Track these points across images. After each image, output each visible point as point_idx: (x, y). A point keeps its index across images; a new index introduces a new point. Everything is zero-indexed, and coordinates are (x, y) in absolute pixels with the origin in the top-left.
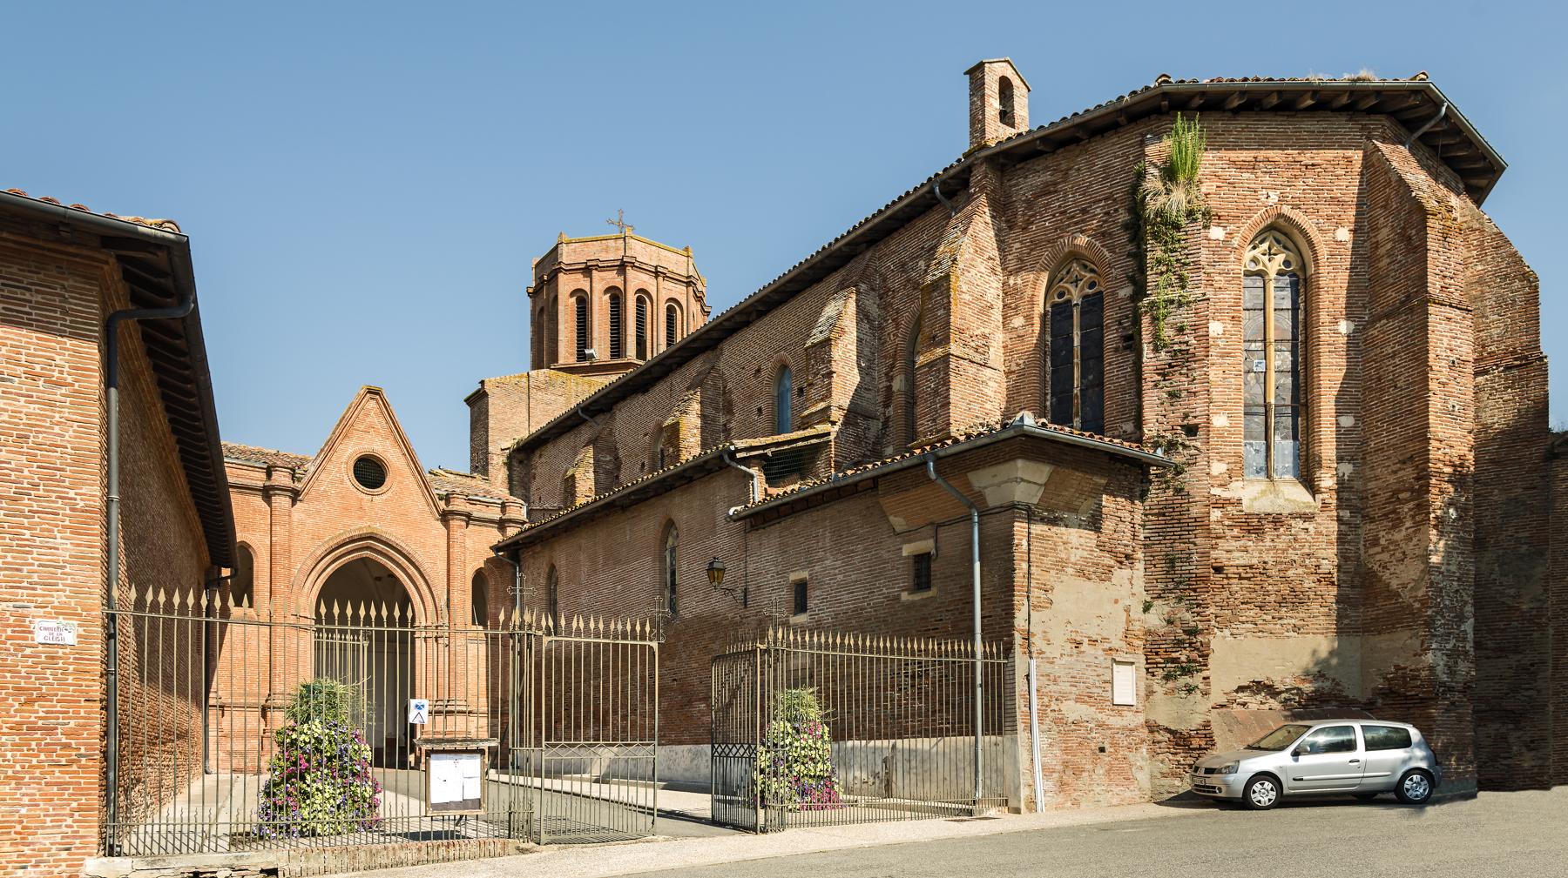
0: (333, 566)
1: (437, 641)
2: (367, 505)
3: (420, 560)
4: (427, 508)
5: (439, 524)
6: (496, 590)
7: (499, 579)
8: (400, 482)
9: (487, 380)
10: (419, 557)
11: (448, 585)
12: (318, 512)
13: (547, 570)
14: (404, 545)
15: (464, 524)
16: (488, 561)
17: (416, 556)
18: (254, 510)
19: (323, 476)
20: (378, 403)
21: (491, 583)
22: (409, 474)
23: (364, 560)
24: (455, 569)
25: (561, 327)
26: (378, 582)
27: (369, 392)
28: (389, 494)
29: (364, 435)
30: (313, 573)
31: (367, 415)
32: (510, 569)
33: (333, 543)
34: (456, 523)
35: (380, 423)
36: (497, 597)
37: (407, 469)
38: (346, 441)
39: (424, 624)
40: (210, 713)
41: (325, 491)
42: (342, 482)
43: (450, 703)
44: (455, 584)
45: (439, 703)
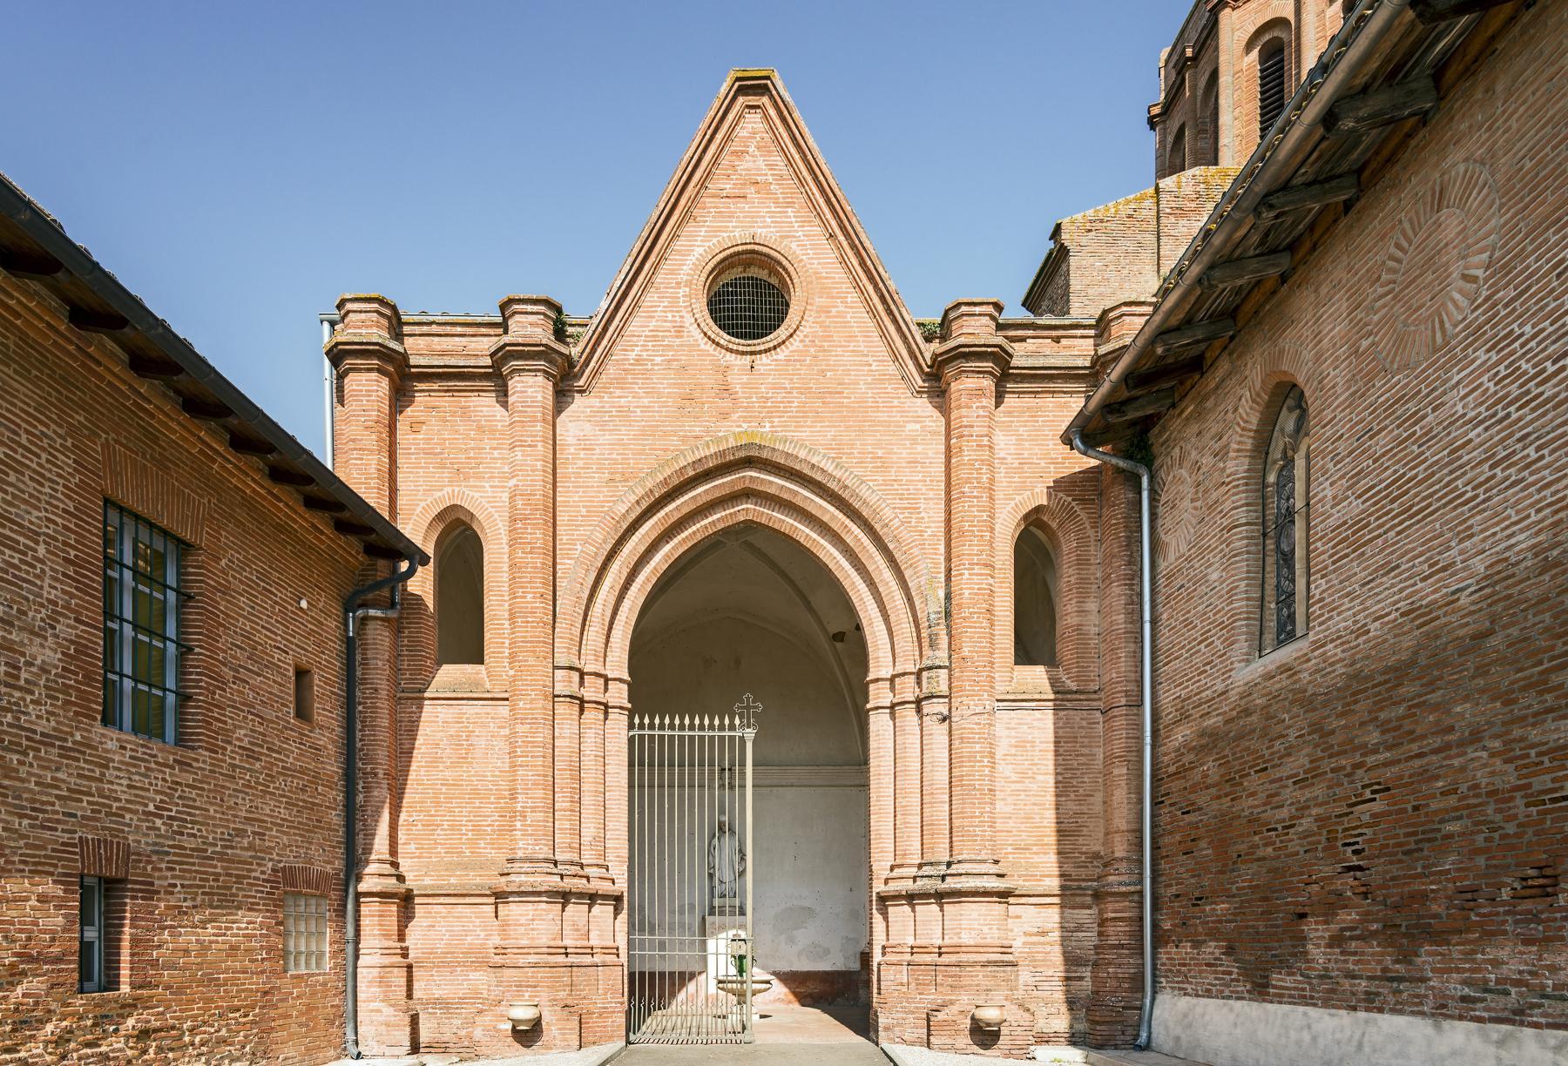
0: (667, 548)
1: (919, 710)
2: (738, 380)
3: (873, 499)
4: (892, 369)
5: (924, 406)
6: (1082, 562)
7: (1091, 533)
8: (825, 310)
9: (1065, 221)
10: (870, 494)
11: (949, 559)
12: (624, 413)
13: (1254, 420)
14: (830, 468)
15: (988, 383)
16: (1063, 486)
17: (863, 492)
18: (480, 429)
19: (635, 325)
20: (766, 117)
21: (1068, 546)
22: (846, 286)
23: (750, 526)
24: (969, 511)
25: (1225, 118)
26: (839, 645)
27: (742, 91)
28: (795, 344)
29: (733, 205)
30: (615, 566)
31: (740, 154)
32: (1121, 494)
33: (653, 481)
34: (971, 386)
35: (771, 167)
36: (1083, 582)
37: (840, 274)
38: (689, 229)
39: (887, 672)
40: (364, 909)
41: (638, 361)
42: (679, 331)
43: (954, 869)
44: (967, 549)
45: (927, 870)
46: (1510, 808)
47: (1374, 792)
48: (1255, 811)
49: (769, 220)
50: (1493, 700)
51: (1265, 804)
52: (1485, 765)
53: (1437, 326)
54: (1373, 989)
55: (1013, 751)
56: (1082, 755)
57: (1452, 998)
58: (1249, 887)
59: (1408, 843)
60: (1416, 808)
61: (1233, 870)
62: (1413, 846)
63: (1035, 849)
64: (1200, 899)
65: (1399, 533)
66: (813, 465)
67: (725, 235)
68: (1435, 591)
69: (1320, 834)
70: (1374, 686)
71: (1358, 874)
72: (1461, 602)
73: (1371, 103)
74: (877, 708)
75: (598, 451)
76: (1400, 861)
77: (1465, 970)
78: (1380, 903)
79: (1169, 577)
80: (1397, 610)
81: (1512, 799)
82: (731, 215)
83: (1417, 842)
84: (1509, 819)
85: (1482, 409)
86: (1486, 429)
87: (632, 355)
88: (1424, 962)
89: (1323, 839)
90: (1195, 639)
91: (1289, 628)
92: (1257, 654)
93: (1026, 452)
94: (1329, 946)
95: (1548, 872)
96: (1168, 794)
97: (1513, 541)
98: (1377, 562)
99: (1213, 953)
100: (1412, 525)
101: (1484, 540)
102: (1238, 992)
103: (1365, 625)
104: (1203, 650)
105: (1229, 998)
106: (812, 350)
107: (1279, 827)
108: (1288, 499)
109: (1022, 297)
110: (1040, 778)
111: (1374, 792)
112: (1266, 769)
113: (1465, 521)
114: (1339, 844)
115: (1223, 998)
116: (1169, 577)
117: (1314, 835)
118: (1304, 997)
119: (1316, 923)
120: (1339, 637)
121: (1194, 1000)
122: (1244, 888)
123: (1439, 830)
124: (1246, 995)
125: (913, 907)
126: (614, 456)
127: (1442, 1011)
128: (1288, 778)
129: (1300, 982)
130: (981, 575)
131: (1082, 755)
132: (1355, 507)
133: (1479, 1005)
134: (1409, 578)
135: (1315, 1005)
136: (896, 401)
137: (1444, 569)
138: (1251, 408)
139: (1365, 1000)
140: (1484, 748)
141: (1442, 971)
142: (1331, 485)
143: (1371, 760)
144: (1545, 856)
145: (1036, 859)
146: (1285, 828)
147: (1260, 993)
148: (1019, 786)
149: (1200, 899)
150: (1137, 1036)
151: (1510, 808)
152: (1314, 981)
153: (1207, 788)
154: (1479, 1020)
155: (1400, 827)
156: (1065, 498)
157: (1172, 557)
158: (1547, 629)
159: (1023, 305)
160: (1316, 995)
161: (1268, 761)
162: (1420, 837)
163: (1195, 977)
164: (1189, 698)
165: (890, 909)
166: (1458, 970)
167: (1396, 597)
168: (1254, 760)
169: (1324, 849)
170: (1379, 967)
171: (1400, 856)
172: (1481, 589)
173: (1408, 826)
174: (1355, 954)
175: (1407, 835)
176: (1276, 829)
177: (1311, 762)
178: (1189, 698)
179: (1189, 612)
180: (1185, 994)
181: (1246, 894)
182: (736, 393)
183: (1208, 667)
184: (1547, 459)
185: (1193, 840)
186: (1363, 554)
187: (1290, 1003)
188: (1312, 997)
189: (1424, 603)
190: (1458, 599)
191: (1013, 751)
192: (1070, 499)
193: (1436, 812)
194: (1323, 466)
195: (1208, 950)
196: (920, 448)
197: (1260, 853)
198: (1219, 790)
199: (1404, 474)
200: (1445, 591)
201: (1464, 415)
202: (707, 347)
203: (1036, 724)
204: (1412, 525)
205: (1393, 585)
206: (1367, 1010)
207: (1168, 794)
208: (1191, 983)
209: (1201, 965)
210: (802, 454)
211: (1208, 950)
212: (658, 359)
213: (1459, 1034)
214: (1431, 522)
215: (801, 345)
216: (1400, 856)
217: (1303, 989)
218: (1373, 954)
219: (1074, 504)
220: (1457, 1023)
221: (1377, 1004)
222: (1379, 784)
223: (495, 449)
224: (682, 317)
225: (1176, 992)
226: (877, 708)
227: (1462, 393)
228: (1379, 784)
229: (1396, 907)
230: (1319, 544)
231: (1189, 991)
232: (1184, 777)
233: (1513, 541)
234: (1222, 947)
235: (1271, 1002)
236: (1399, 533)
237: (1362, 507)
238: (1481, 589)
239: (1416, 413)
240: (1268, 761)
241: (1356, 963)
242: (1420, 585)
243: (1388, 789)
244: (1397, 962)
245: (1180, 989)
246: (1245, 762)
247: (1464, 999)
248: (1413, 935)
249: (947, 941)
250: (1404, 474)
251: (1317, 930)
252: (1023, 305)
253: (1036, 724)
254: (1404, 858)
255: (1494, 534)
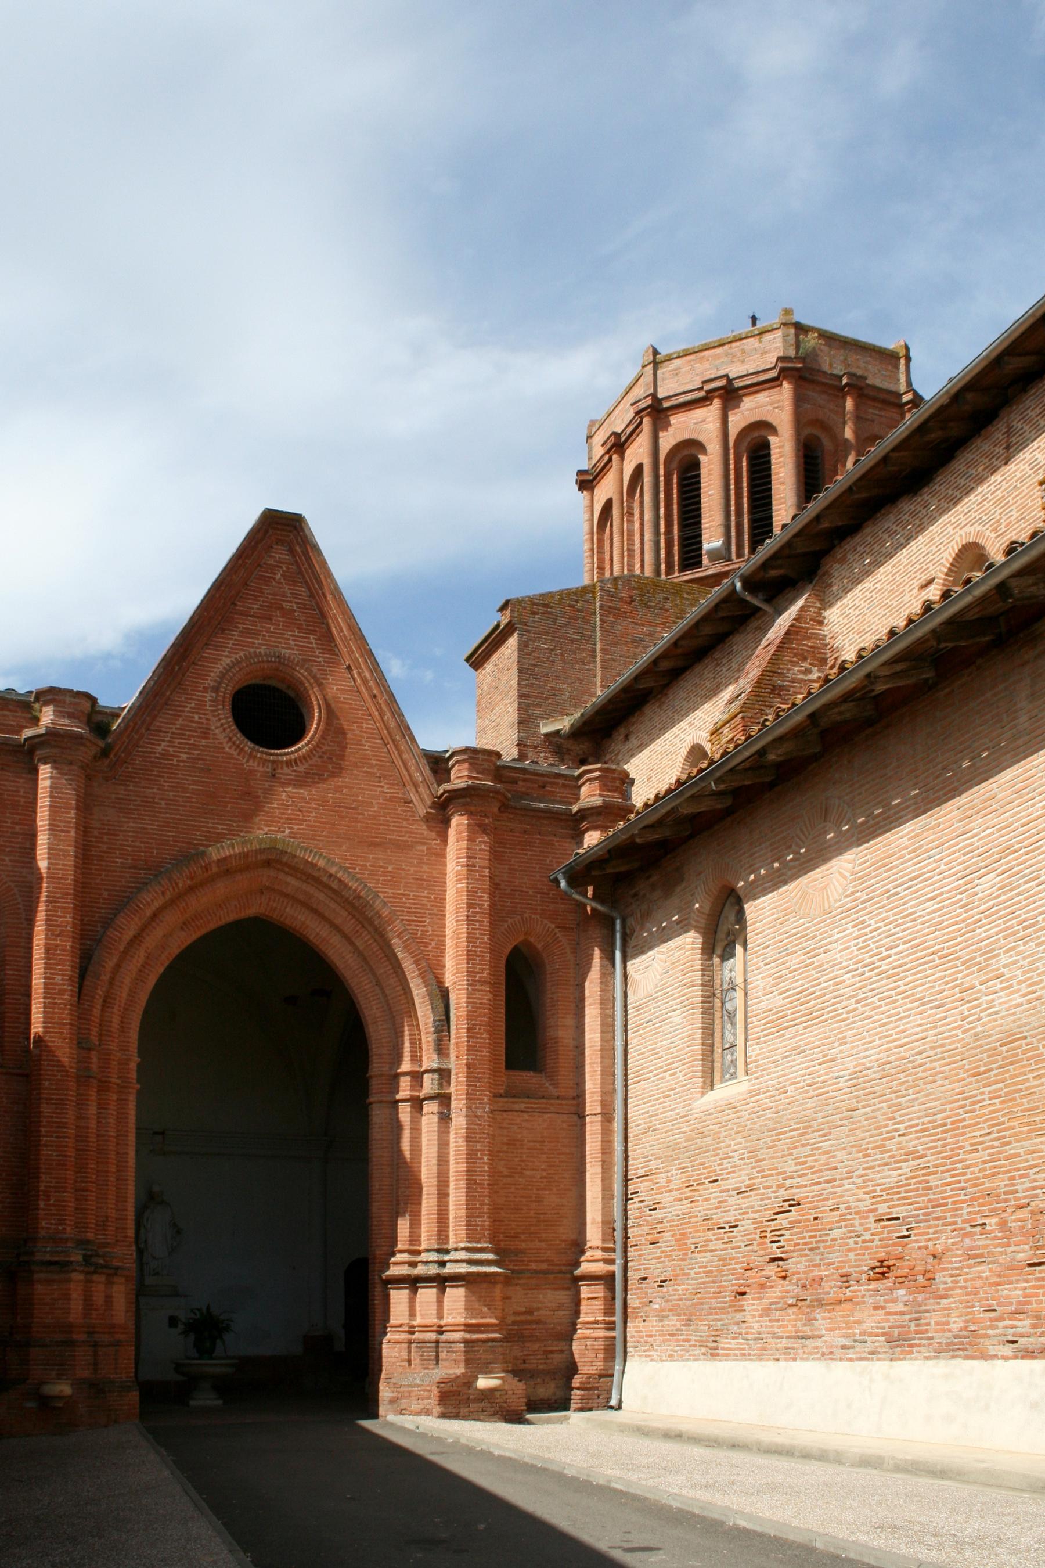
35: (295, 595)
46: (867, 1223)
47: (790, 1205)
48: (709, 1212)
49: (292, 643)
50: (858, 1152)
51: (716, 1208)
52: (854, 1195)
53: (825, 897)
54: (790, 1345)
55: (505, 1148)
56: (563, 1154)
57: (837, 1347)
58: (705, 1272)
59: (811, 1243)
60: (816, 1219)
61: (691, 1259)
62: (814, 1245)
63: (523, 1237)
64: (664, 1281)
65: (805, 1028)
66: (331, 875)
67: (252, 650)
68: (826, 1074)
69: (756, 1234)
70: (791, 1131)
71: (781, 1263)
72: (840, 1084)
73: (785, 746)
74: (381, 1102)
75: (121, 837)
76: (807, 1255)
77: (843, 1328)
78: (794, 1284)
79: (638, 1008)
80: (804, 1080)
81: (867, 1217)
82: (258, 633)
83: (816, 1242)
84: (867, 1230)
85: (851, 962)
86: (853, 977)
87: (159, 749)
88: (820, 1325)
89: (757, 1237)
90: (661, 1067)
91: (732, 1071)
92: (709, 1088)
93: (517, 881)
94: (761, 1316)
95: (885, 1264)
96: (637, 1192)
97: (867, 1053)
98: (792, 1044)
99: (674, 1325)
100: (813, 1025)
101: (853, 1048)
102: (694, 1355)
103: (784, 1086)
104: (669, 1078)
105: (688, 1360)
106: (330, 766)
107: (727, 1226)
108: (731, 971)
109: (468, 652)
110: (528, 1173)
111: (790, 1205)
112: (716, 1181)
113: (842, 1032)
114: (768, 1241)
115: (683, 1361)
116: (638, 1008)
117: (751, 1234)
118: (744, 1355)
119: (753, 1299)
120: (768, 1091)
121: (660, 1364)
122: (700, 1273)
123: (828, 1235)
124: (702, 1357)
125: (442, 1291)
126: (137, 844)
127: (828, 1355)
128: (734, 1189)
129: (741, 1344)
130: (482, 991)
131: (563, 1154)
132: (778, 1001)
133: (851, 1351)
134: (812, 1061)
135: (751, 1360)
136: (405, 823)
137: (831, 1061)
138: (704, 897)
139: (784, 1354)
140: (853, 1183)
141: (830, 1330)
142: (763, 978)
143: (788, 1182)
144: (884, 1254)
145: (524, 1246)
146: (730, 1227)
147: (712, 1355)
148: (509, 1180)
149: (664, 1281)
150: (609, 1399)
151: (867, 1223)
152: (751, 1342)
153: (670, 1191)
154: (851, 1360)
155: (807, 1232)
156: (549, 925)
157: (641, 993)
158: (884, 1114)
159: (467, 660)
160: (752, 1352)
161: (719, 1175)
162: (819, 1239)
163: (660, 1346)
164: (656, 1115)
165: (448, 1289)
166: (840, 1329)
167: (804, 1071)
168: (709, 1173)
169: (759, 1245)
170: (793, 1329)
171: (807, 1252)
172: (851, 1079)
173: (811, 1231)
174: (778, 1321)
175: (811, 1237)
176: (724, 1228)
177: (750, 1179)
178: (656, 1115)
179: (656, 1043)
180: (652, 1360)
181: (702, 1278)
182: (259, 797)
183: (671, 1093)
184: (884, 1009)
185: (659, 1233)
186: (783, 1035)
187: (734, 1360)
188: (749, 1354)
189: (820, 1079)
190: (839, 1083)
191: (505, 1148)
192: (553, 926)
193: (828, 1223)
194: (756, 963)
195: (671, 1323)
196: (425, 868)
197: (712, 1245)
198: (681, 1194)
199: (807, 989)
200: (832, 1075)
201: (841, 963)
202: (232, 751)
203: (524, 1124)
204: (813, 1025)
205: (802, 1063)
206: (786, 1360)
207: (637, 1192)
208: (657, 1351)
209: (665, 1335)
210: (321, 863)
211: (671, 1323)
212: (184, 756)
213: (841, 1369)
214: (824, 1026)
215: (319, 760)
216: (807, 1252)
217: (743, 1349)
218: (789, 1321)
219: (557, 930)
220: (839, 1363)
221: (792, 1356)
222: (793, 1200)
223: (17, 824)
224: (208, 719)
225: (644, 1359)
226: (381, 1102)
227: (840, 947)
228: (793, 1200)
229: (804, 1286)
230: (754, 1019)
231: (655, 1357)
232: (651, 1180)
233: (867, 1053)
234: (682, 1320)
235: (720, 1361)
236: (805, 1028)
237: (782, 1002)
238: (851, 1079)
239: (814, 949)
240: (719, 1175)
241: (779, 1327)
242: (818, 1067)
243: (799, 1204)
244: (805, 1325)
245: (646, 1356)
246: (702, 1174)
247: (843, 1347)
248: (814, 1306)
249: (418, 1321)
250: (807, 989)
251: (753, 1305)
252: (467, 660)
253: (524, 1124)
254: (809, 1253)
255: (858, 1046)
